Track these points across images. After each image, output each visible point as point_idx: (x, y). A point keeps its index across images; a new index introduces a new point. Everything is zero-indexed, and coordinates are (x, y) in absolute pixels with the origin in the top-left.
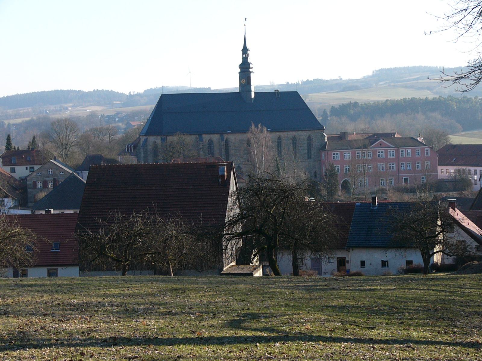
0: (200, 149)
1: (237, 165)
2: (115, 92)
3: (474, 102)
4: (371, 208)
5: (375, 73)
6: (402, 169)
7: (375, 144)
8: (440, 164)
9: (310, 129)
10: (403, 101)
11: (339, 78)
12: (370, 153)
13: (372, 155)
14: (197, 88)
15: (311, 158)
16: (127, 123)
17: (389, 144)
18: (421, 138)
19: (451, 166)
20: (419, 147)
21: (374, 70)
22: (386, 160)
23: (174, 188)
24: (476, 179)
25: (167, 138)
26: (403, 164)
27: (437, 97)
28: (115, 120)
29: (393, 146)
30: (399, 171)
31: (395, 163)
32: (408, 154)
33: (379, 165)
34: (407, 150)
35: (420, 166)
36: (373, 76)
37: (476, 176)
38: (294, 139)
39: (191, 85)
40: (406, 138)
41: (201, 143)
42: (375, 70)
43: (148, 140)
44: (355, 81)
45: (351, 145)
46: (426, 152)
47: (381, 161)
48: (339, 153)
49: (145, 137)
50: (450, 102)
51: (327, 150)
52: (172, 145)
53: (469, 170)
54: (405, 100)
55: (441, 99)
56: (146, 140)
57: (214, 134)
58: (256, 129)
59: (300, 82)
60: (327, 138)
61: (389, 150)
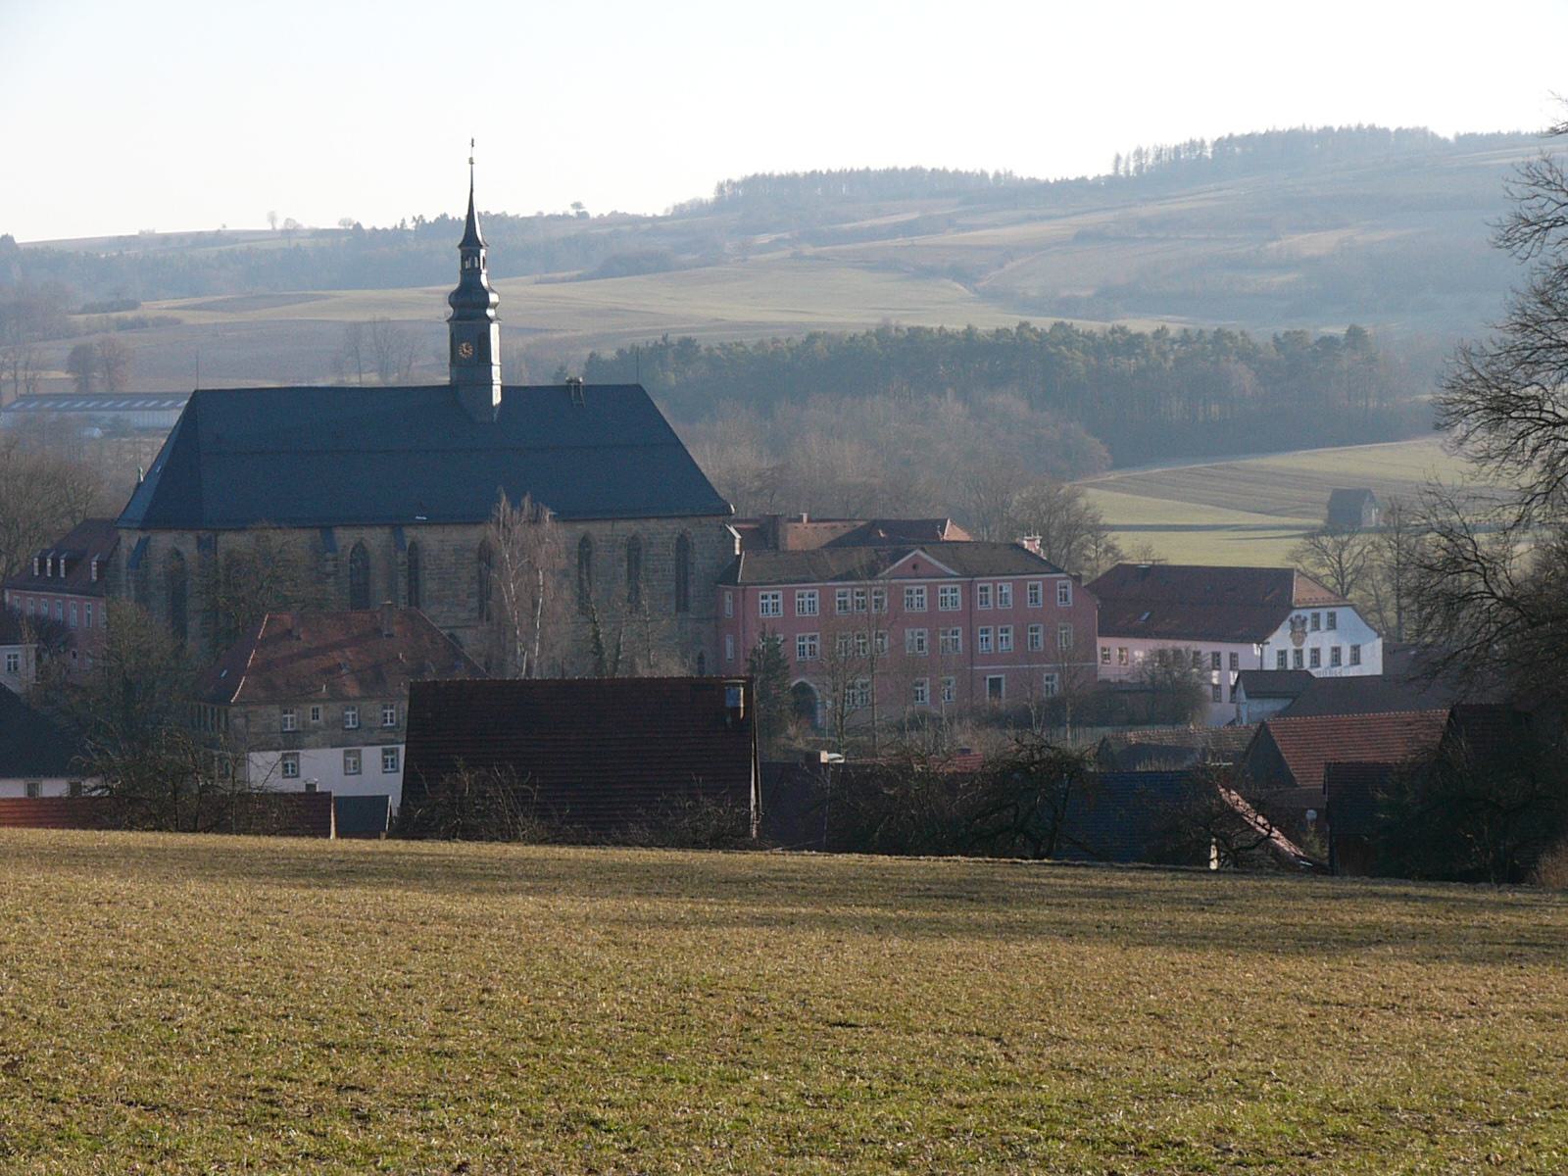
0: (328, 575)
3: (1154, 352)
6: (982, 648)
7: (897, 565)
8: (1105, 632)
10: (875, 340)
11: (572, 212)
12: (881, 593)
13: (886, 604)
18: (1034, 540)
19: (1137, 637)
21: (724, 178)
24: (1215, 681)
25: (219, 538)
26: (987, 631)
29: (956, 574)
30: (972, 654)
32: (1003, 598)
37: (1215, 673)
38: (634, 550)
41: (329, 555)
46: (1061, 594)
48: (780, 593)
49: (142, 535)
51: (741, 584)
54: (882, 334)
55: (1028, 334)
56: (143, 544)
57: (371, 526)
60: (741, 540)
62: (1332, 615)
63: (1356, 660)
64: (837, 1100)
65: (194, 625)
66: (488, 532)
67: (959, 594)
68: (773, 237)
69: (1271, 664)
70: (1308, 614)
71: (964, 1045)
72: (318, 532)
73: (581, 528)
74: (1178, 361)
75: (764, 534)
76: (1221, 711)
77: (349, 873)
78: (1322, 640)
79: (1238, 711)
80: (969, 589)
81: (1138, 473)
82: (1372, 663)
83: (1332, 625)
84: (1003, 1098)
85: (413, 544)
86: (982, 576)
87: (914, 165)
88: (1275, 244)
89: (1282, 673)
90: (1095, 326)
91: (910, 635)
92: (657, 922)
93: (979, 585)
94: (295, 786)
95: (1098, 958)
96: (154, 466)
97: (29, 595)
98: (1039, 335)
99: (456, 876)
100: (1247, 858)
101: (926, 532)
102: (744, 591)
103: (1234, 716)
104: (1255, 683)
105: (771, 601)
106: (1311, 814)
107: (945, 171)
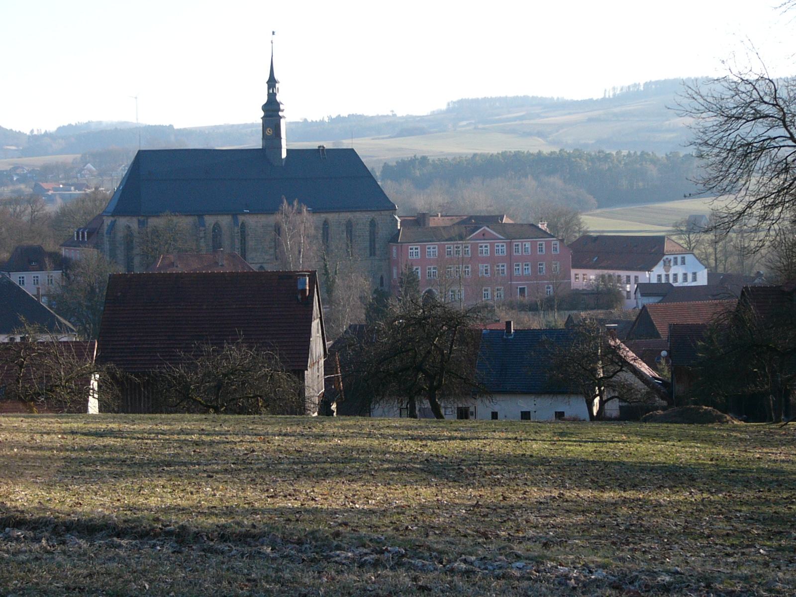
0: (201, 238)
1: (259, 265)
2: (7, 130)
3: (615, 160)
4: (505, 337)
5: (451, 106)
6: (515, 273)
7: (475, 234)
8: (576, 266)
9: (373, 209)
11: (390, 114)
14: (149, 126)
15: (375, 254)
16: (36, 185)
17: (497, 235)
18: (544, 224)
20: (543, 239)
22: (492, 260)
23: (234, 307)
24: (628, 290)
26: (518, 265)
27: (557, 150)
28: (12, 180)
29: (502, 237)
31: (505, 264)
33: (482, 267)
34: (524, 243)
35: (544, 268)
36: (449, 111)
37: (628, 286)
38: (349, 226)
39: (137, 119)
40: (522, 225)
41: (201, 228)
42: (452, 101)
43: (117, 223)
44: (419, 118)
45: (435, 235)
47: (484, 260)
49: (112, 219)
50: (578, 159)
51: (401, 243)
52: (155, 231)
53: (619, 276)
55: (563, 153)
56: (113, 224)
58: (290, 209)
59: (326, 120)
60: (401, 222)
61: (496, 244)
62: (683, 259)
63: (695, 279)
66: (278, 217)
67: (505, 247)
68: (468, 122)
69: (654, 280)
70: (672, 257)
72: (196, 218)
74: (626, 164)
79: (637, 303)
80: (510, 245)
81: (608, 210)
82: (702, 280)
83: (683, 263)
85: (243, 224)
86: (516, 239)
87: (525, 94)
88: (667, 122)
89: (659, 285)
93: (514, 244)
96: (120, 186)
97: (72, 249)
98: (568, 154)
102: (401, 246)
103: (635, 305)
104: (645, 289)
105: (414, 251)
106: (664, 353)
107: (537, 97)
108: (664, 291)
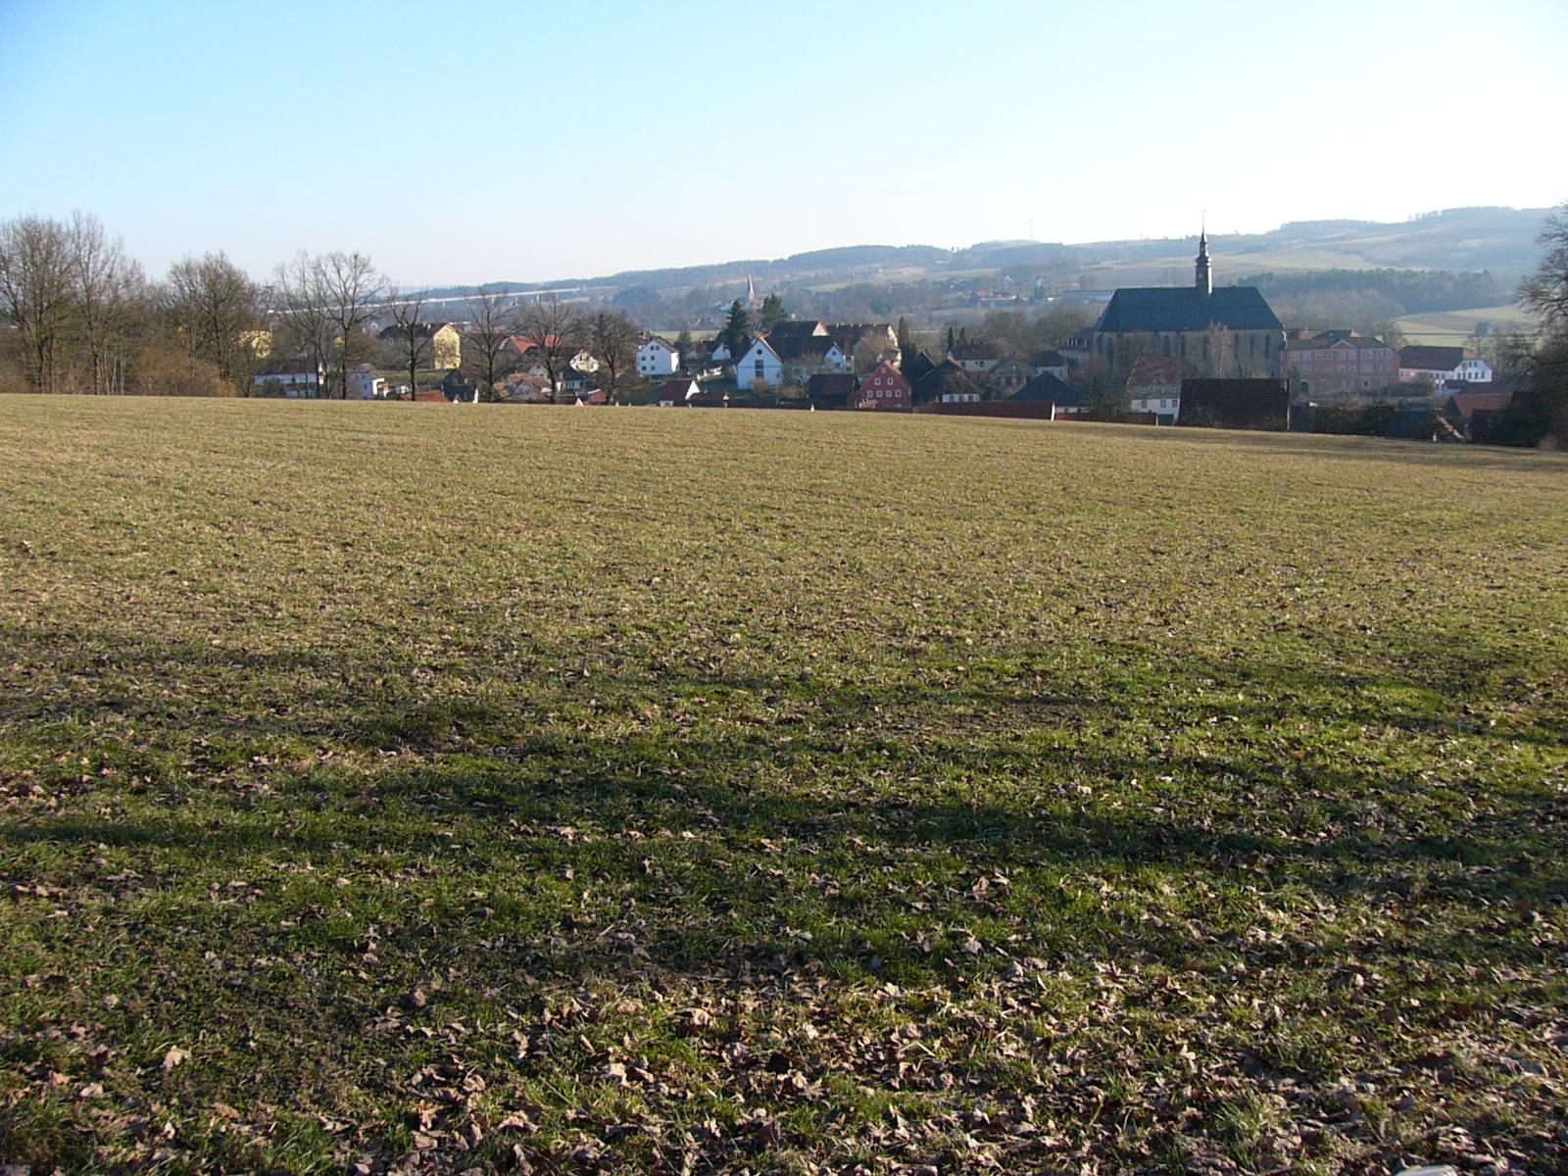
8: (1403, 366)
36: (1282, 230)
47: (1341, 362)
54: (1333, 271)
64: (1319, 506)
65: (1115, 361)
71: (1357, 492)
73: (1235, 332)
75: (1294, 334)
76: (1439, 392)
77: (1164, 436)
78: (1472, 370)
82: (1488, 378)
84: (1370, 508)
89: (1459, 381)
90: (1401, 269)
91: (1339, 367)
92: (1259, 452)
94: (1145, 410)
95: (1399, 467)
99: (1196, 437)
100: (1445, 438)
101: (1346, 334)
104: (1450, 384)
108: (1461, 385)
